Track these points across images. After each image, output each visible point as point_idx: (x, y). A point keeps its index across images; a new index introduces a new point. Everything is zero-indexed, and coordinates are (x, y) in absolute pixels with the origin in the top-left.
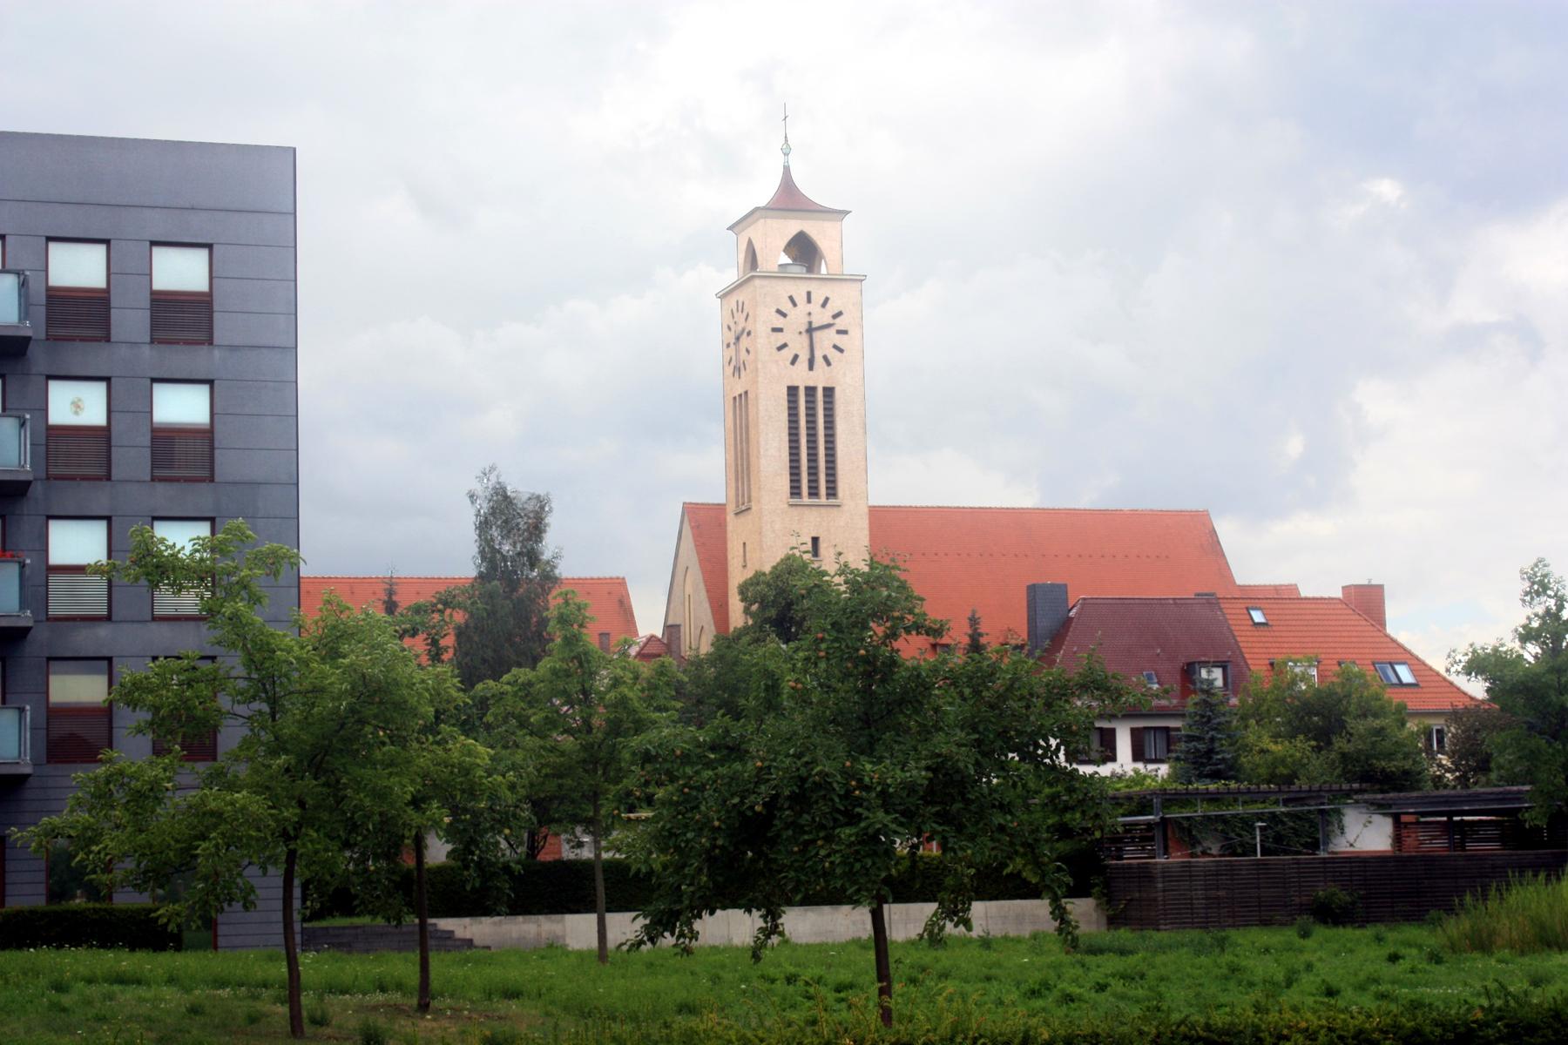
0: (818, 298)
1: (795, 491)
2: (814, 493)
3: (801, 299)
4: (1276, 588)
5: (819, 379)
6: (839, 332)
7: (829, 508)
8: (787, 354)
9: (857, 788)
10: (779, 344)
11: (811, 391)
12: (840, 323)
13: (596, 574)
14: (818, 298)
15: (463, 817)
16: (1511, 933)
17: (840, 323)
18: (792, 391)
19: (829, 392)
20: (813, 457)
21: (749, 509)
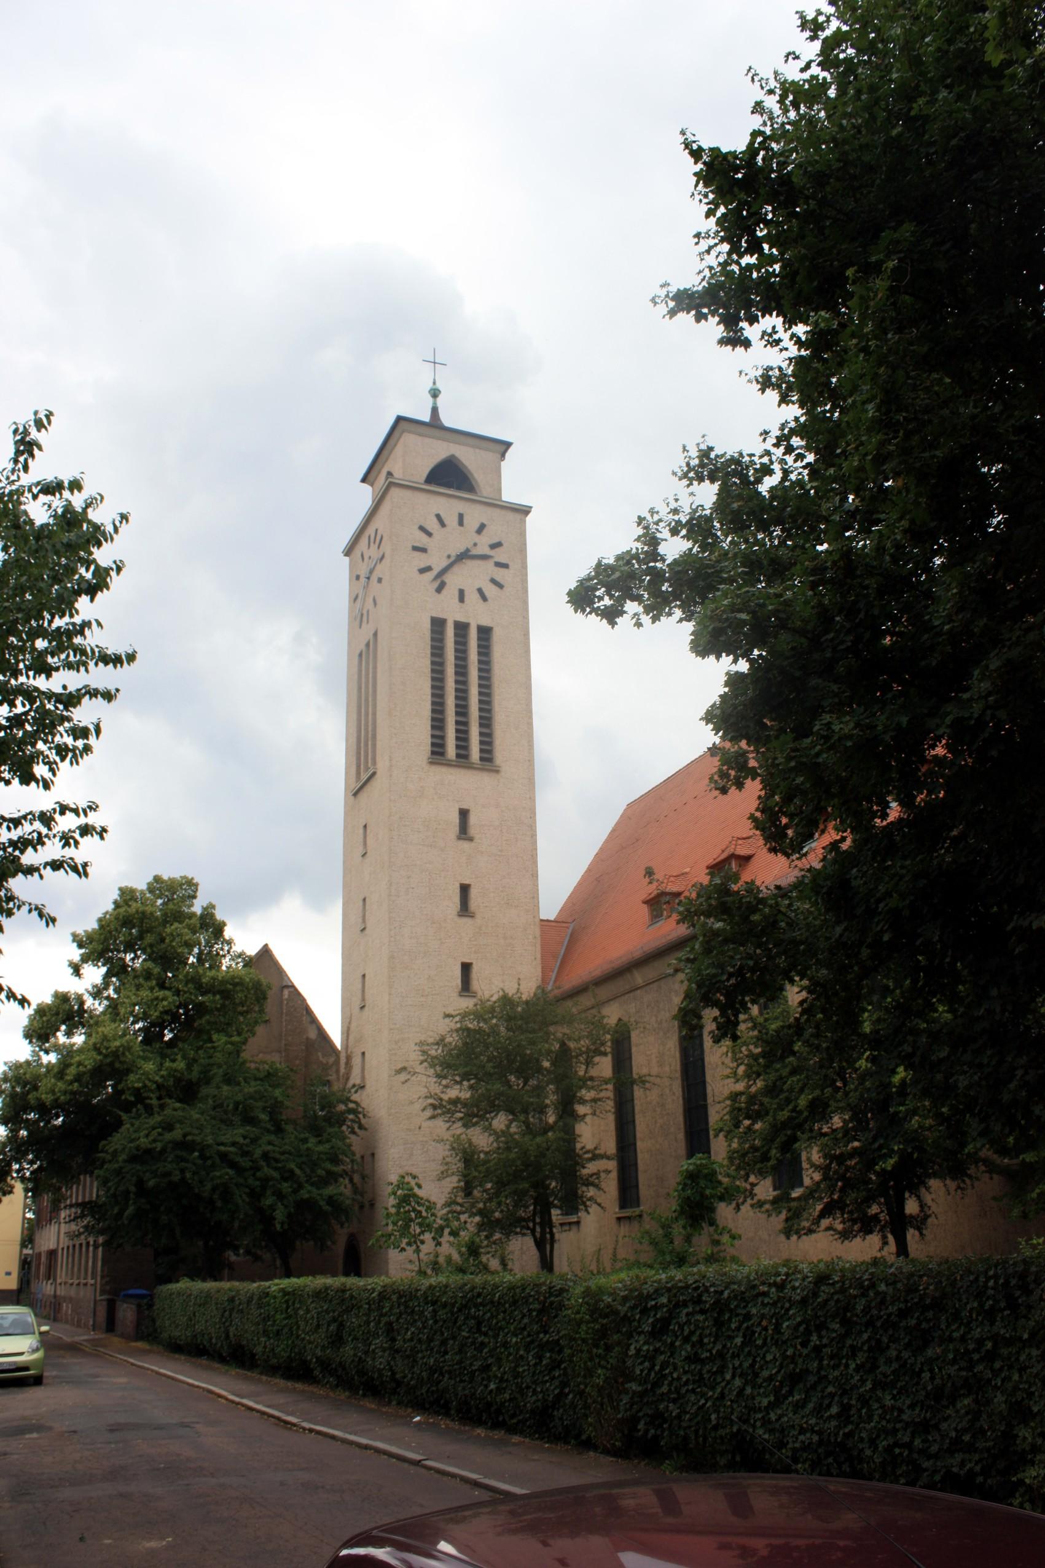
0: (471, 523)
1: (437, 750)
2: (463, 754)
3: (451, 520)
4: (342, 1034)
5: (476, 615)
6: (499, 565)
7: (368, 788)
8: (490, 590)
9: (752, 974)
10: (423, 566)
11: (461, 628)
12: (500, 555)
13: (621, 812)
14: (471, 523)
15: (512, 1078)
16: (864, 1274)
17: (500, 555)
18: (438, 625)
19: (485, 633)
20: (462, 710)
21: (374, 774)
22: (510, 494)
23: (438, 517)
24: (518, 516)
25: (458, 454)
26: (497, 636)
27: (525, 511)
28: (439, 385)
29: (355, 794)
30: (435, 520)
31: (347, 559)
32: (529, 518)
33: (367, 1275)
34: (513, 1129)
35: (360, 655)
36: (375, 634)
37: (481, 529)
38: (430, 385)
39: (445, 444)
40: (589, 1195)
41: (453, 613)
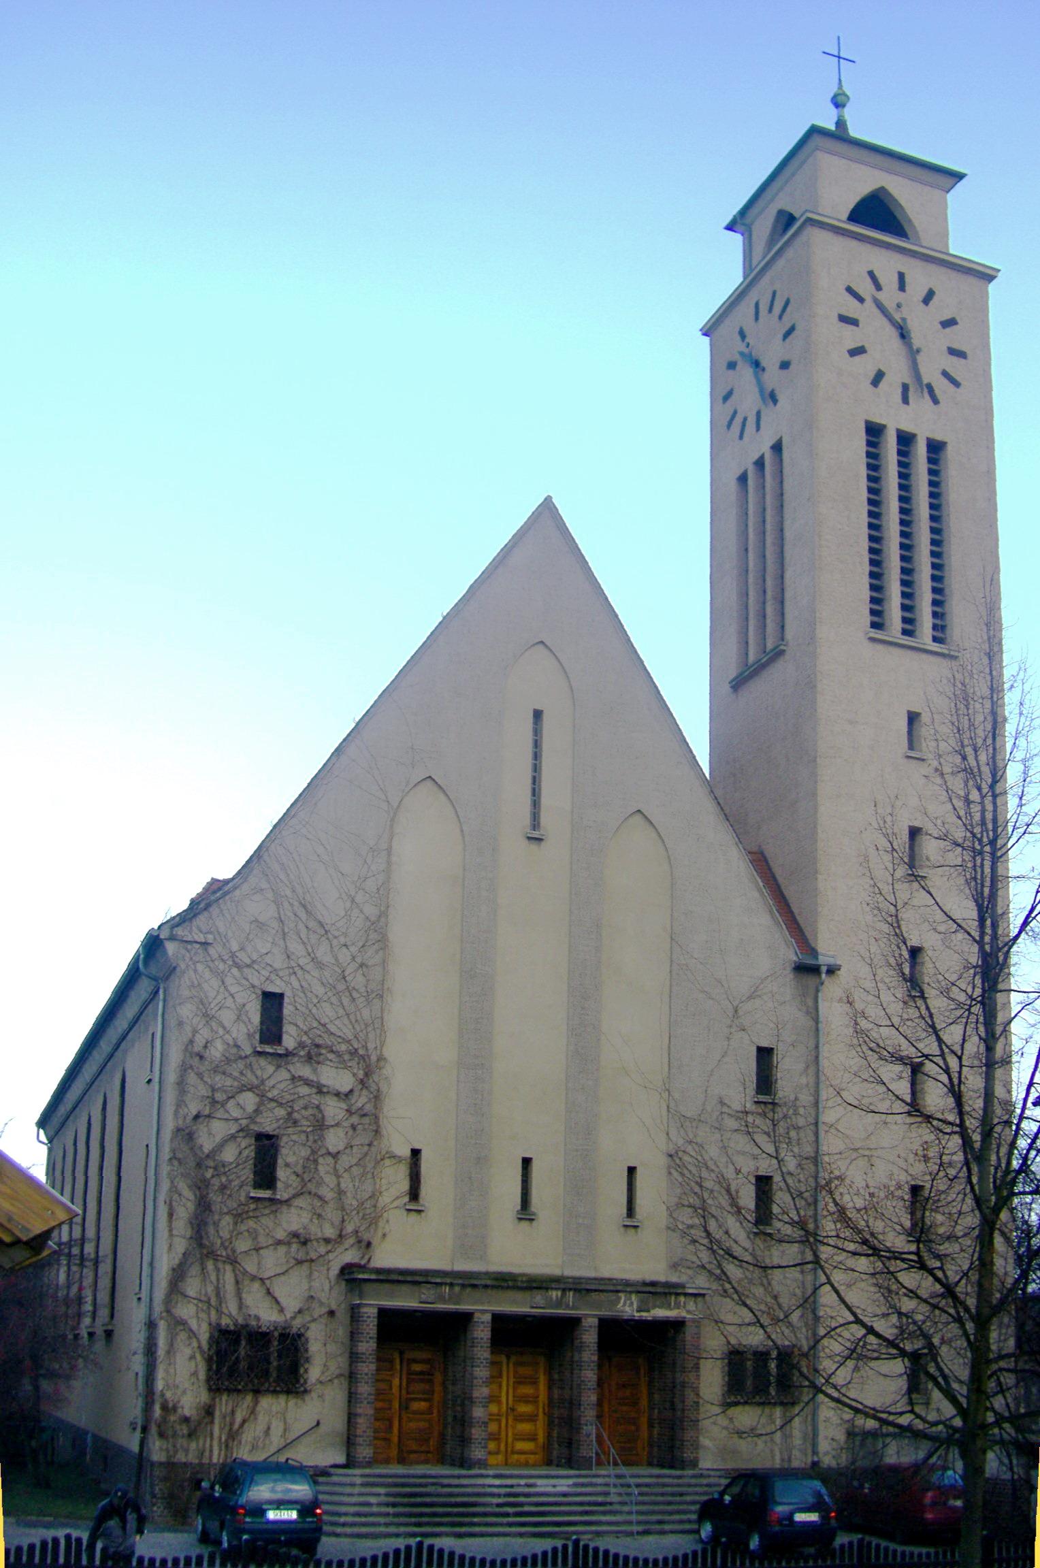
11: (906, 440)
18: (874, 432)
19: (936, 448)
22: (958, 247)
23: (871, 274)
24: (981, 283)
25: (780, 207)
26: (950, 453)
27: (987, 276)
28: (847, 89)
29: (738, 684)
30: (895, 278)
31: (707, 339)
32: (992, 287)
33: (382, 1359)
34: (229, 1155)
35: (743, 479)
36: (777, 448)
37: (928, 297)
38: (835, 89)
39: (877, 173)
40: (331, 1231)
41: (896, 419)
